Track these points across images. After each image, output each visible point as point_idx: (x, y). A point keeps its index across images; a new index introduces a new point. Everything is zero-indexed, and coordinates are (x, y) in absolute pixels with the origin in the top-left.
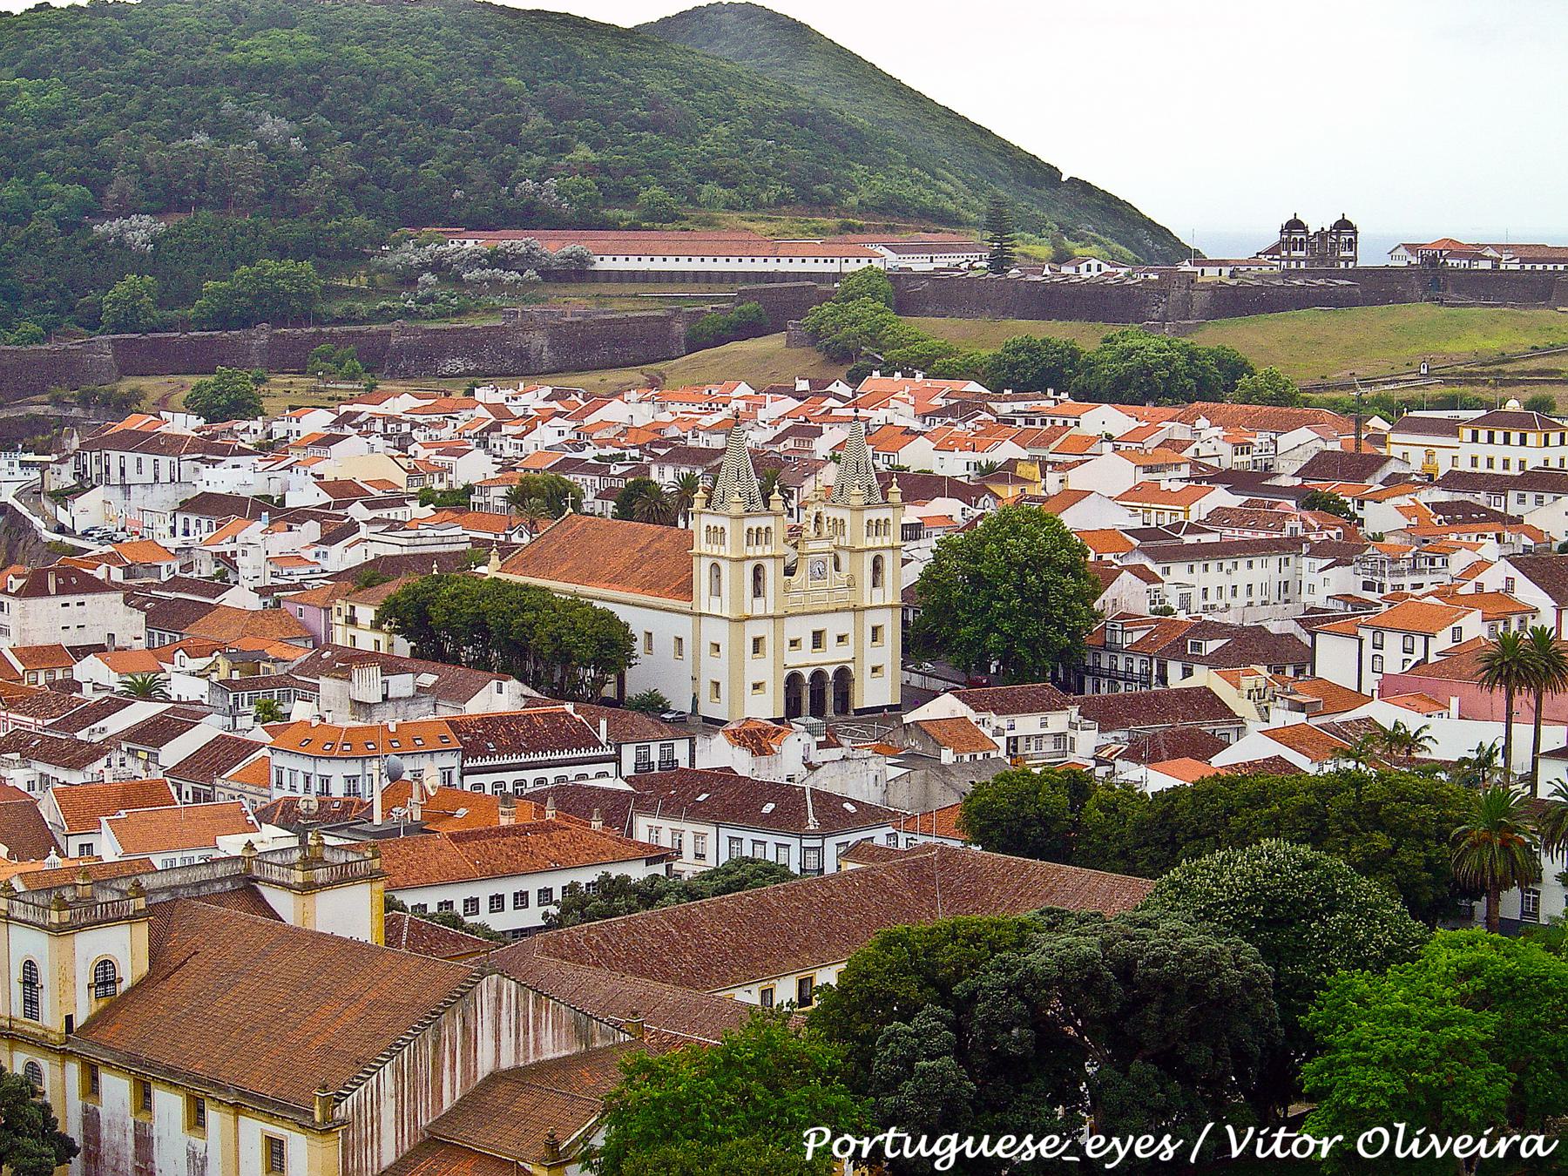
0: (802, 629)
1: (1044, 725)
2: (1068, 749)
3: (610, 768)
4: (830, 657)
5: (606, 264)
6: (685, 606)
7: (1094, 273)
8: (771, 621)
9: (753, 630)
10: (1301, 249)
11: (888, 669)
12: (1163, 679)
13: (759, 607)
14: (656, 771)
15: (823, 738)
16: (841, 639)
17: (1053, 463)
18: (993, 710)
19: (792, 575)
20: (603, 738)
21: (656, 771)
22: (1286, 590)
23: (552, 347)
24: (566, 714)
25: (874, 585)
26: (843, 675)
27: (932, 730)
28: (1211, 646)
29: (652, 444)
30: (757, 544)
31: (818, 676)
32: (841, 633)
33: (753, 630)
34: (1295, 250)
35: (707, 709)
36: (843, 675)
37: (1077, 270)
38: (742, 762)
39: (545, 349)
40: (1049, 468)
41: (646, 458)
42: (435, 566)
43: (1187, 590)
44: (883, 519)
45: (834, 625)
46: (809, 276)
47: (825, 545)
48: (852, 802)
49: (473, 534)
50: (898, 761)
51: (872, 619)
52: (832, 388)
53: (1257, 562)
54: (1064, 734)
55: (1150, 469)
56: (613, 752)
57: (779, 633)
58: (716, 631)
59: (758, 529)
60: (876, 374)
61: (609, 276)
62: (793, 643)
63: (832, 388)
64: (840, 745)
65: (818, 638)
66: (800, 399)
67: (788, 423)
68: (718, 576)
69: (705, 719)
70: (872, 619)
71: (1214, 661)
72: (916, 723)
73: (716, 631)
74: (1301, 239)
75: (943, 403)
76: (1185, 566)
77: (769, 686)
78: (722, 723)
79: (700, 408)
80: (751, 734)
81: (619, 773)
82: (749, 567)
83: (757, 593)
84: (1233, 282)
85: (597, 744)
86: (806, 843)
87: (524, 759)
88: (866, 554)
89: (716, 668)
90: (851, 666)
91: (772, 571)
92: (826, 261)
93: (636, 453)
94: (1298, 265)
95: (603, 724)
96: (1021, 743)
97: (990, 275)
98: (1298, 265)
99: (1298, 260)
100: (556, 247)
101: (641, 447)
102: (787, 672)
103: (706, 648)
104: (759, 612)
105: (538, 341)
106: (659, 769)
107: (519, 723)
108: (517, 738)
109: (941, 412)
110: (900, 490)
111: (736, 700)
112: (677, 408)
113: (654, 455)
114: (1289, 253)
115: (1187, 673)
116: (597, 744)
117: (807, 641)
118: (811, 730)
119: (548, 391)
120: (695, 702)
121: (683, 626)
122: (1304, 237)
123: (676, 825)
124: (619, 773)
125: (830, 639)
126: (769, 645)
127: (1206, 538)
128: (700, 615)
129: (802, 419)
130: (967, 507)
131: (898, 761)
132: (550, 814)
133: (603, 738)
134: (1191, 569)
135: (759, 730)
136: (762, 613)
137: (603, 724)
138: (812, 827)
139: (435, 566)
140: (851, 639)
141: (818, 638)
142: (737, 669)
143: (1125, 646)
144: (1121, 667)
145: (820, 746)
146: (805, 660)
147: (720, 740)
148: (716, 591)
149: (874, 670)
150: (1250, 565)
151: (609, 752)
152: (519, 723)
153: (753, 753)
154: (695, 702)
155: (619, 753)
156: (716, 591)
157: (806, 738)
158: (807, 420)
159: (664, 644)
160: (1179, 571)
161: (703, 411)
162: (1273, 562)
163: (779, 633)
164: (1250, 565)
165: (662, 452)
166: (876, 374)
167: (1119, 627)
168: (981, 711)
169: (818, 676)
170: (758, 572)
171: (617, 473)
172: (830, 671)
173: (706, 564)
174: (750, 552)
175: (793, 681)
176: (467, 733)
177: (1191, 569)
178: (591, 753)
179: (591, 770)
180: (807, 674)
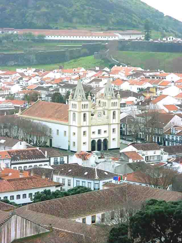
0: (95, 129)
2: (161, 159)
3: (48, 163)
4: (103, 136)
5: (48, 38)
6: (66, 123)
7: (171, 40)
8: (88, 127)
9: (83, 129)
11: (116, 139)
13: (85, 124)
14: (59, 164)
15: (100, 156)
16: (105, 132)
17: (159, 88)
18: (142, 149)
19: (93, 116)
20: (46, 156)
21: (59, 164)
24: (37, 150)
25: (113, 118)
26: (105, 141)
27: (126, 154)
29: (60, 83)
30: (87, 108)
31: (99, 141)
33: (83, 129)
35: (72, 149)
36: (105, 141)
37: (167, 39)
38: (80, 162)
40: (158, 89)
41: (58, 87)
42: (5, 113)
44: (115, 102)
45: (103, 128)
47: (101, 108)
48: (107, 172)
49: (15, 105)
50: (119, 162)
51: (112, 127)
52: (105, 69)
54: (160, 156)
56: (48, 159)
57: (89, 130)
58: (74, 130)
59: (114, 103)
60: (116, 66)
62: (93, 133)
63: (105, 69)
64: (104, 158)
65: (99, 132)
66: (97, 72)
67: (93, 78)
68: (75, 116)
69: (71, 151)
70: (112, 127)
72: (123, 153)
73: (74, 130)
75: (132, 73)
77: (87, 143)
78: (75, 152)
79: (72, 74)
80: (82, 155)
81: (50, 164)
82: (82, 114)
83: (85, 120)
85: (44, 157)
86: (96, 182)
88: (111, 111)
89: (74, 139)
90: (107, 138)
91: (88, 115)
92: (104, 37)
93: (56, 85)
95: (46, 152)
96: (149, 158)
100: (36, 33)
101: (57, 84)
103: (72, 134)
104: (114, 122)
105: (33, 57)
106: (60, 164)
107: (25, 152)
108: (24, 156)
109: (131, 75)
110: (120, 95)
111: (79, 147)
112: (66, 74)
113: (60, 86)
116: (44, 157)
117: (97, 132)
118: (97, 154)
119: (34, 69)
120: (69, 147)
121: (66, 128)
123: (64, 177)
124: (50, 164)
125: (102, 132)
126: (87, 133)
128: (70, 125)
129: (97, 77)
130: (137, 99)
131: (119, 162)
133: (46, 156)
135: (84, 154)
136: (85, 125)
137: (46, 152)
138: (96, 178)
139: (5, 113)
140: (107, 132)
142: (79, 139)
144: (175, 139)
145: (99, 158)
146: (96, 137)
148: (74, 120)
149: (113, 139)
151: (47, 159)
152: (25, 152)
153: (83, 160)
154: (69, 147)
155: (50, 160)
156: (74, 120)
157: (96, 156)
158: (98, 77)
159: (61, 132)
161: (73, 75)
163: (89, 130)
165: (62, 85)
166: (116, 66)
168: (139, 150)
169: (99, 141)
171: (51, 90)
172: (102, 140)
173: (72, 113)
174: (83, 110)
175: (93, 142)
176: (12, 154)
179: (43, 164)
180: (96, 140)
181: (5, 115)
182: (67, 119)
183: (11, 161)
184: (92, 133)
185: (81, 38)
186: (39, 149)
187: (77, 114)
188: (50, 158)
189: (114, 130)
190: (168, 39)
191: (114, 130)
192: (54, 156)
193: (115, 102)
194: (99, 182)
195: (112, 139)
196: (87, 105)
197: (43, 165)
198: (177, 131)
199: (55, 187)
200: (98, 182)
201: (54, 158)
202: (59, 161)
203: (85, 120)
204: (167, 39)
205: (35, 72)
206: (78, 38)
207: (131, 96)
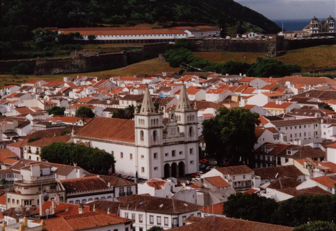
1: (244, 178)
5: (99, 38)
10: (317, 27)
12: (279, 163)
16: (180, 153)
22: (317, 134)
23: (86, 64)
28: (293, 153)
31: (174, 164)
32: (181, 151)
34: (315, 27)
36: (182, 164)
39: (84, 65)
40: (241, 98)
43: (285, 135)
45: (178, 148)
46: (165, 40)
48: (187, 203)
53: (307, 126)
55: (272, 98)
56: (112, 190)
61: (103, 42)
62: (166, 155)
65: (173, 153)
71: (295, 157)
74: (332, 23)
76: (285, 128)
82: (152, 131)
83: (155, 140)
84: (296, 38)
85: (107, 188)
87: (85, 193)
90: (184, 161)
94: (316, 32)
97: (221, 38)
98: (316, 32)
99: (316, 31)
102: (165, 164)
103: (140, 157)
114: (313, 28)
115: (287, 161)
117: (170, 154)
119: (86, 77)
120: (137, 174)
122: (333, 23)
126: (159, 155)
127: (290, 119)
132: (94, 210)
134: (287, 128)
141: (173, 153)
143: (267, 153)
147: (146, 184)
148: (142, 139)
149: (191, 162)
150: (305, 126)
154: (137, 174)
156: (142, 139)
160: (283, 129)
162: (312, 125)
164: (305, 126)
167: (265, 147)
169: (174, 164)
170: (155, 133)
172: (178, 163)
177: (287, 128)
178: (106, 190)
179: (106, 196)
180: (170, 164)
181: (55, 135)
182: (133, 139)
183: (66, 195)
184: (164, 155)
185: (142, 37)
186: (101, 177)
187: (146, 132)
188: (114, 188)
189: (191, 150)
190: (249, 35)
191: (191, 150)
192: (119, 185)
193: (179, 116)
194: (178, 216)
195: (189, 162)
196: (157, 120)
197: (106, 197)
198: (268, 149)
199: (124, 224)
200: (176, 216)
201: (127, 188)
202: (125, 191)
203: (155, 140)
204: (247, 36)
205: (87, 80)
206: (138, 37)
207: (209, 107)
